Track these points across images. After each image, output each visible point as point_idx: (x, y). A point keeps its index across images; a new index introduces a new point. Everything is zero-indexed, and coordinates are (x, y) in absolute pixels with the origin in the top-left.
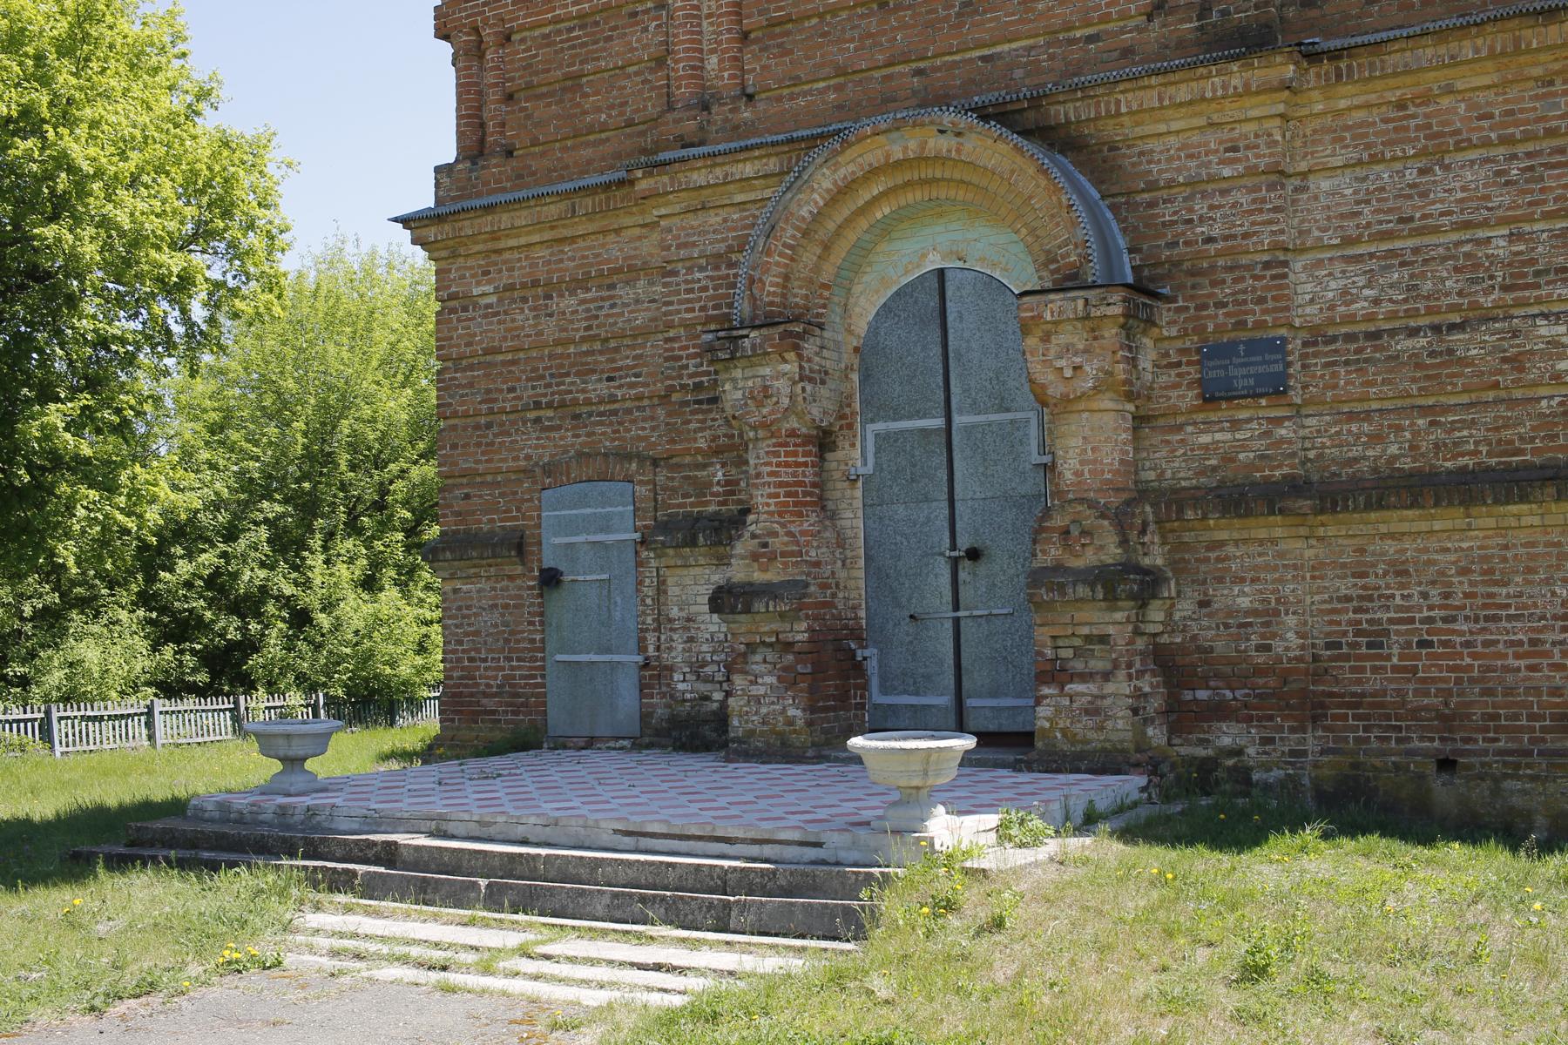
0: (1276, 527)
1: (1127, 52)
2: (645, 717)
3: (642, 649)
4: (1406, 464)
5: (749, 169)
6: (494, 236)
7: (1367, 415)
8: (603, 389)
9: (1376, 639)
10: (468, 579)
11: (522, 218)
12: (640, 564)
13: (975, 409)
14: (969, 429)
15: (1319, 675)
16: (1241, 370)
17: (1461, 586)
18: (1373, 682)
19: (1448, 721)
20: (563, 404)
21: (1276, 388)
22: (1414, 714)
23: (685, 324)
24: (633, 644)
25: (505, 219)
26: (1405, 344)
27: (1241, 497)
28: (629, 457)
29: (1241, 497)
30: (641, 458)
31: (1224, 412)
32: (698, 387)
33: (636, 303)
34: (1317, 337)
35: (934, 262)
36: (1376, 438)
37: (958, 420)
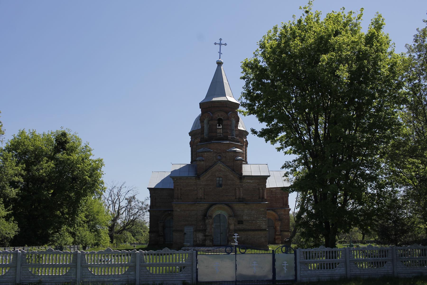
16: (240, 222)
21: (242, 223)
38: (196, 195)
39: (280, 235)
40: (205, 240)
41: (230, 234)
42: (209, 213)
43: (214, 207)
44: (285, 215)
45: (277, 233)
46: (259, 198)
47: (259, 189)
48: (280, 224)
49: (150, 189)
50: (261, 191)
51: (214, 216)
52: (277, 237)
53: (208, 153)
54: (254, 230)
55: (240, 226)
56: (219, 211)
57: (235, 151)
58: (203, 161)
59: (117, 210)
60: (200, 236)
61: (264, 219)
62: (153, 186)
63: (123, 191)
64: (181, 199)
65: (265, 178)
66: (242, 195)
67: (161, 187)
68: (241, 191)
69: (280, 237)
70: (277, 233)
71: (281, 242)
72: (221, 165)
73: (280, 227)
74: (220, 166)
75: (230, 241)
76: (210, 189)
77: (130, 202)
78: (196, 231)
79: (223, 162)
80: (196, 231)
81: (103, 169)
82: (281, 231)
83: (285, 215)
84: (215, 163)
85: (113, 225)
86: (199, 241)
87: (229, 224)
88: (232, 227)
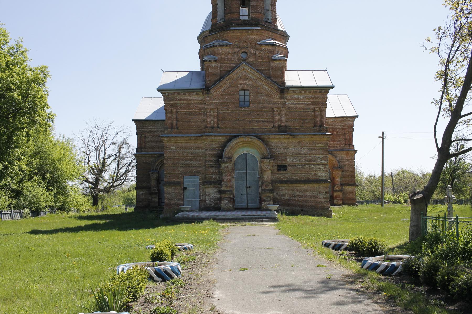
0: (286, 185)
1: (270, 131)
2: (200, 207)
3: (200, 198)
4: (298, 179)
5: (221, 138)
6: (176, 140)
7: (294, 174)
8: (194, 163)
9: (295, 197)
10: (170, 188)
11: (182, 139)
12: (200, 187)
13: (250, 170)
14: (249, 172)
15: (289, 201)
16: (282, 168)
17: (304, 192)
18: (294, 202)
19: (302, 206)
20: (187, 165)
21: (285, 170)
22: (299, 205)
23: (209, 156)
24: (198, 197)
25: (179, 139)
26: (298, 166)
27: (282, 182)
28: (198, 173)
29: (282, 182)
30: (200, 173)
31: (280, 172)
32: (211, 164)
33: (200, 152)
34: (289, 165)
35: (245, 152)
36: (295, 176)
37: (248, 171)
38: (204, 121)
39: (341, 191)
40: (220, 199)
41: (264, 187)
42: (226, 153)
43: (235, 141)
44: (348, 160)
45: (336, 188)
46: (315, 126)
47: (314, 110)
48: (340, 173)
49: (137, 122)
50: (318, 113)
51: (235, 157)
52: (335, 194)
53: (225, 48)
54: (304, 182)
55: (282, 175)
56: (243, 149)
57: (272, 45)
58: (216, 61)
59: (102, 160)
60: (212, 192)
61: (324, 162)
62: (143, 116)
63: (111, 132)
64: (177, 128)
65: (324, 91)
66: (284, 120)
67: (153, 119)
68: (283, 113)
69: (340, 193)
70: (336, 188)
71: (341, 202)
72: (247, 68)
73: (341, 178)
74: (245, 70)
75: (264, 201)
76: (228, 110)
77: (120, 148)
78: (205, 183)
79: (250, 64)
80: (205, 183)
81: (48, 83)
82: (342, 185)
83: (348, 160)
84: (237, 66)
85: (97, 180)
86: (210, 201)
87: (262, 171)
88: (267, 176)
